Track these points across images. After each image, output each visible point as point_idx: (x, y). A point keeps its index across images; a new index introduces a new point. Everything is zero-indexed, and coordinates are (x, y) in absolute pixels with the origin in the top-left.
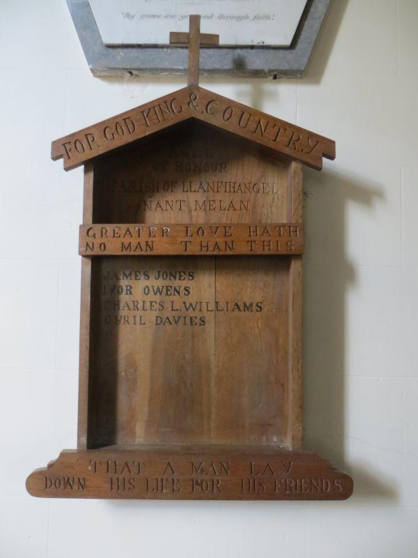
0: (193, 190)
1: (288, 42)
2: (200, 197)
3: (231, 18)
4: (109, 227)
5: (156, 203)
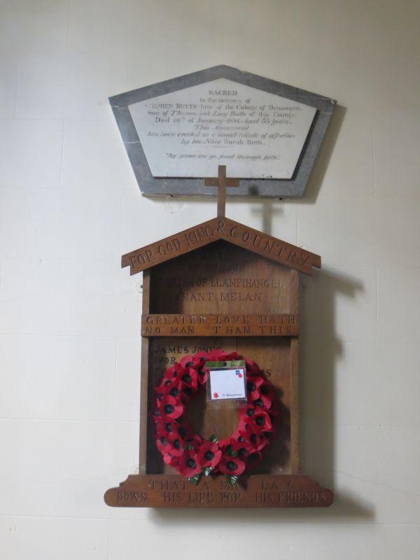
0: (219, 285)
1: (290, 176)
2: (225, 290)
3: (248, 157)
4: (162, 317)
5: (191, 295)
